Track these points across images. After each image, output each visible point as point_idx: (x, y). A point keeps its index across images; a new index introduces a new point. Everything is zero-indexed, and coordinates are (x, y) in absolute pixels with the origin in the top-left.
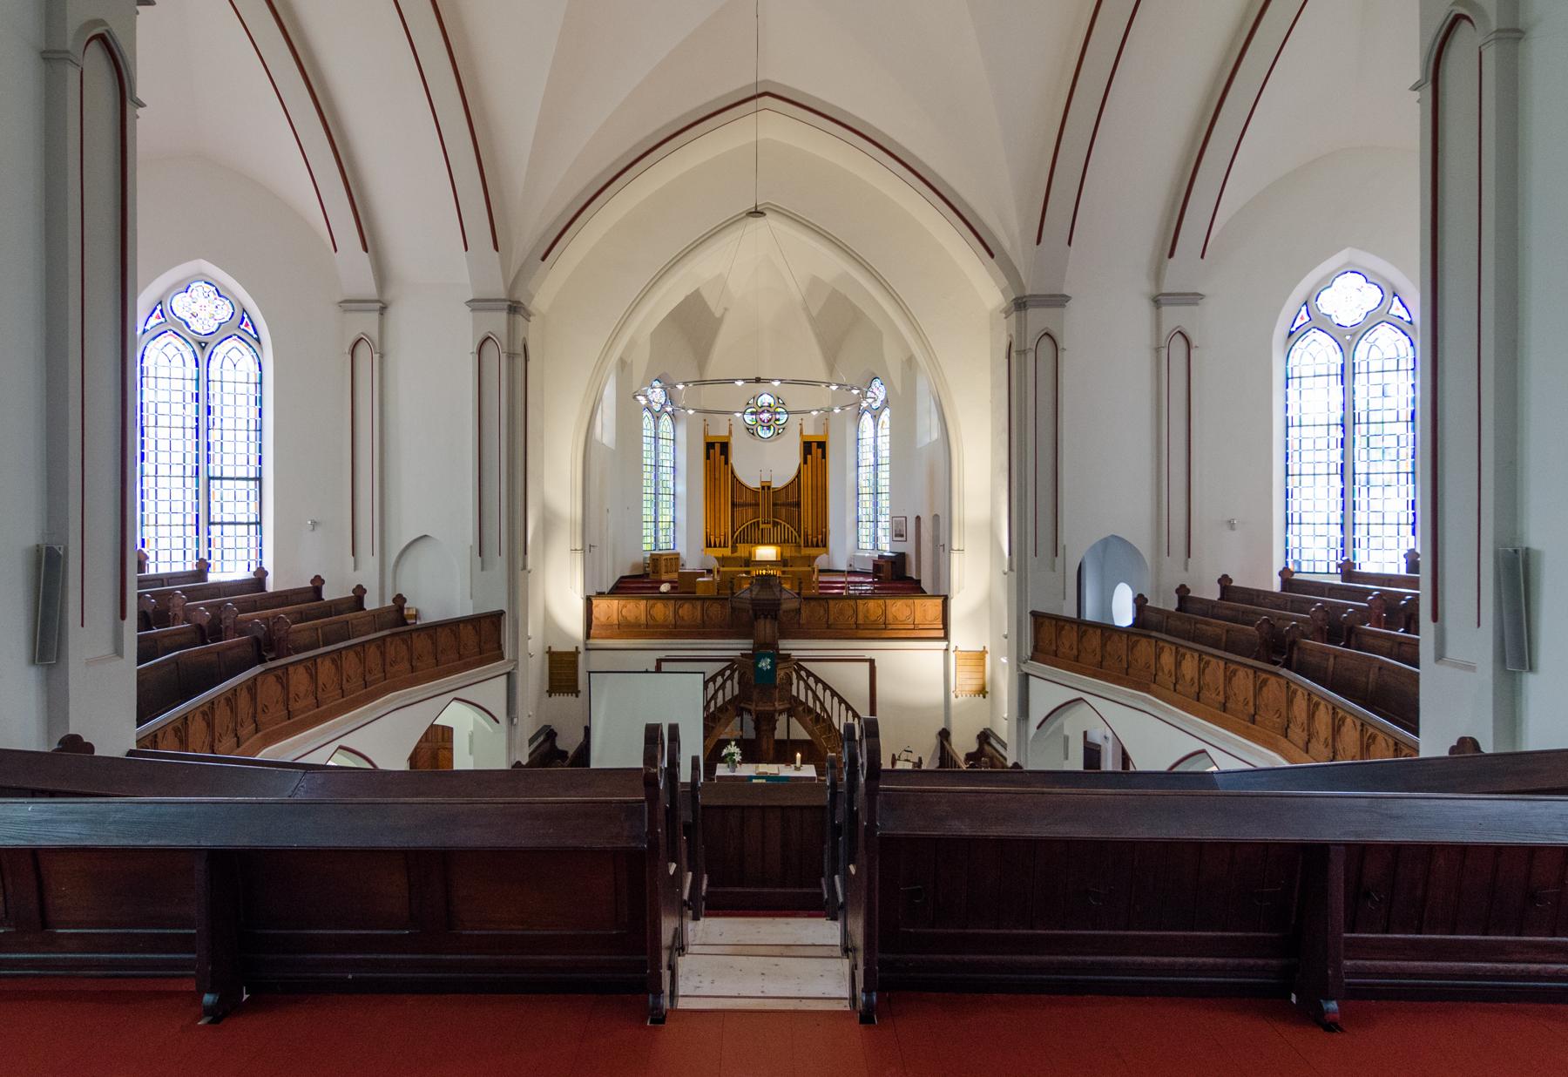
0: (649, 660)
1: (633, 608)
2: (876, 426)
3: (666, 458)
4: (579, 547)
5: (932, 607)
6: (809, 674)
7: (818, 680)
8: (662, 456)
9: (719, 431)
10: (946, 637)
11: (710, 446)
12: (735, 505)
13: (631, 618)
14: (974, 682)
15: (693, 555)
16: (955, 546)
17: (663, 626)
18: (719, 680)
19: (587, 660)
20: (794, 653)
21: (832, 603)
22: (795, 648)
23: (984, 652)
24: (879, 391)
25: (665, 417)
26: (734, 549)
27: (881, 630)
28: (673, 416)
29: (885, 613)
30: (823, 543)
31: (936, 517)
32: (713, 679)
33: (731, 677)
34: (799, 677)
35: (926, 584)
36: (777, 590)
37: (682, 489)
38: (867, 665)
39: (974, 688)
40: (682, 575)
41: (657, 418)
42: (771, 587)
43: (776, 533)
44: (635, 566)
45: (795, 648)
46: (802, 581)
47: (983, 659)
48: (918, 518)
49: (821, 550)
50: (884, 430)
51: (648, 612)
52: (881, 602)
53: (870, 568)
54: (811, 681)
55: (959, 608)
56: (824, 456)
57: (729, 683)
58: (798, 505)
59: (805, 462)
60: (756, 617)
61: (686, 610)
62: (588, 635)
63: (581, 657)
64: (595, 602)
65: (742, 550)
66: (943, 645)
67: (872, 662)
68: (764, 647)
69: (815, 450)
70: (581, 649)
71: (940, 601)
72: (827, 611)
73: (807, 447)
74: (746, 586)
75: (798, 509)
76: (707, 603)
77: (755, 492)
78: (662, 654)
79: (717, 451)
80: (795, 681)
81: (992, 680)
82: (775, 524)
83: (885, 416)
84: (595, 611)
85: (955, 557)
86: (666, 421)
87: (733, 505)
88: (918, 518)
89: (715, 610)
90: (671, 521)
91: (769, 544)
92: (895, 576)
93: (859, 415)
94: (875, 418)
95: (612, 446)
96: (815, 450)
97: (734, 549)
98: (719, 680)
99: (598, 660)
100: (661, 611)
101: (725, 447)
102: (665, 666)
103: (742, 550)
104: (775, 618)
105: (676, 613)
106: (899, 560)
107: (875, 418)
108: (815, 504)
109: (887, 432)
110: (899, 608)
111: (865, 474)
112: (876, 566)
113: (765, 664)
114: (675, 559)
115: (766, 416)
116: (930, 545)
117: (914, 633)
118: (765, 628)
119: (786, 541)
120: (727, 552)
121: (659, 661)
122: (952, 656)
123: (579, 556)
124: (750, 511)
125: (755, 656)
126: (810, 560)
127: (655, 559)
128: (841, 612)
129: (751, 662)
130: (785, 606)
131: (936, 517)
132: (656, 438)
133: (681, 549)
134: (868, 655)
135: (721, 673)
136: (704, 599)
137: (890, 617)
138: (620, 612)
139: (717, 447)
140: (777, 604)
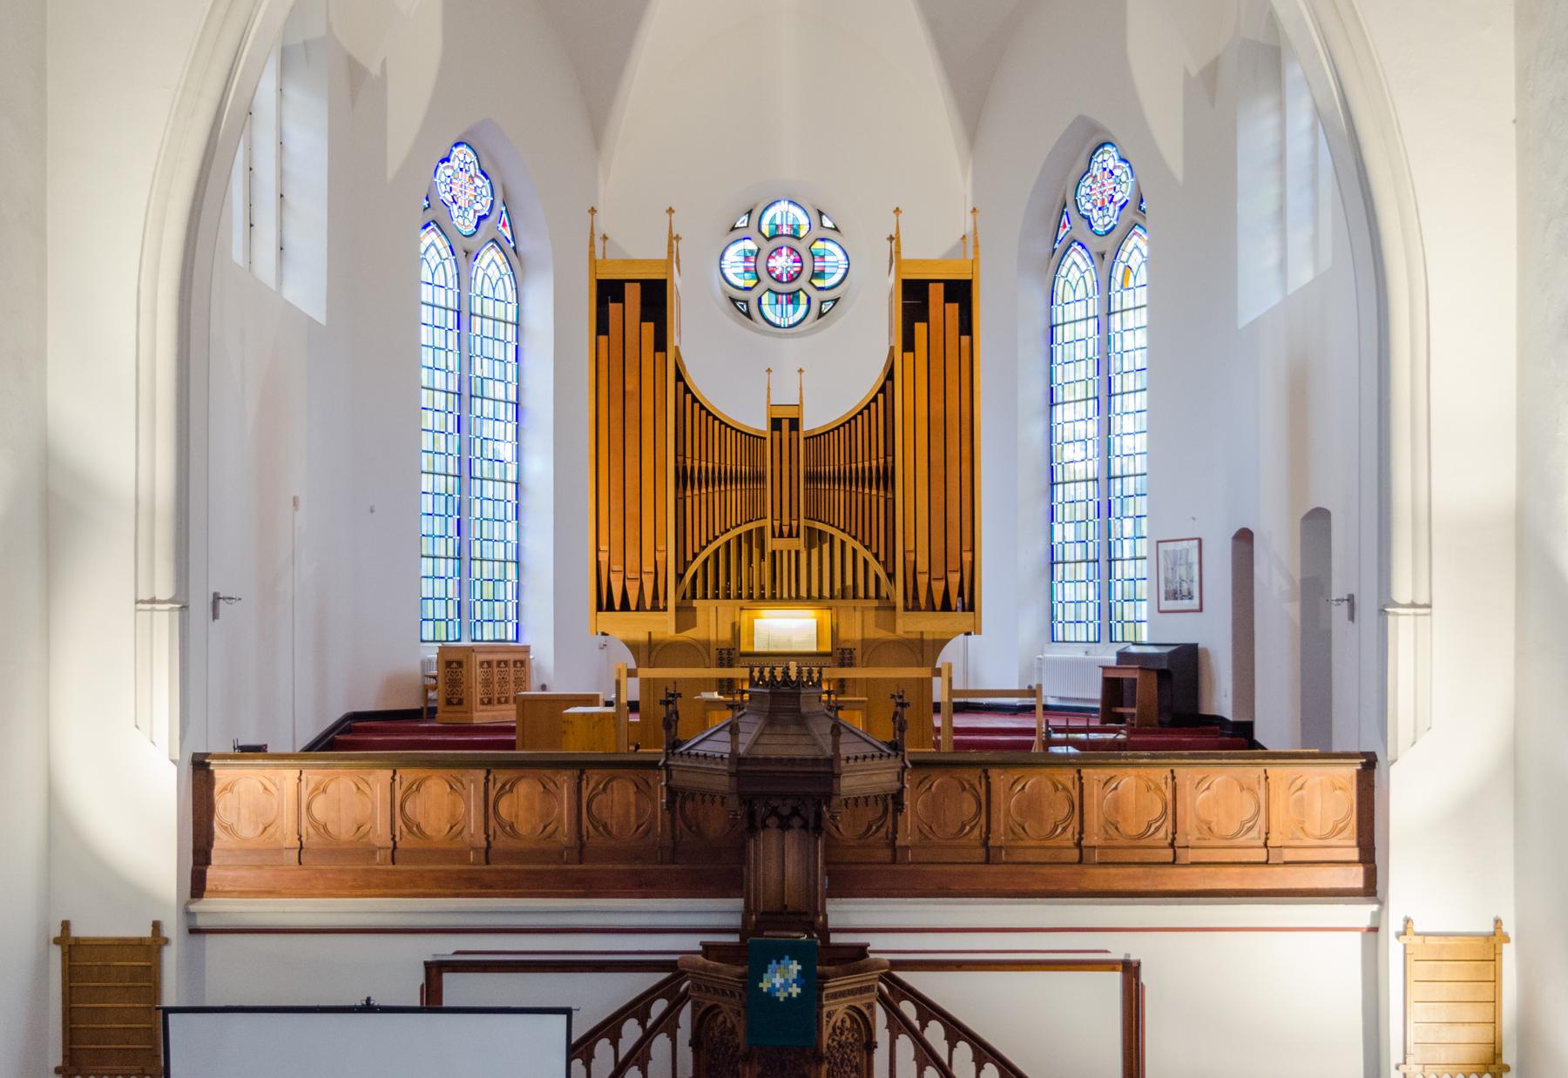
0: (397, 969)
1: (356, 796)
2: (1105, 285)
3: (492, 366)
4: (164, 589)
5: (1325, 792)
6: (929, 1010)
7: (956, 1031)
8: (481, 368)
9: (636, 249)
10: (1371, 889)
11: (609, 291)
12: (701, 488)
13: (343, 830)
14: (1464, 1034)
15: (568, 651)
16: (1402, 590)
17: (446, 855)
18: (631, 1032)
19: (194, 967)
20: (876, 942)
21: (1000, 779)
22: (878, 923)
23: (1495, 938)
24: (1109, 182)
25: (490, 255)
26: (685, 614)
27: (1155, 868)
28: (514, 255)
29: (1172, 811)
30: (962, 598)
31: (1317, 522)
32: (610, 1028)
33: (668, 1023)
34: (898, 1024)
35: (1275, 723)
36: (822, 729)
37: (540, 466)
38: (1115, 978)
39: (1464, 1054)
40: (528, 705)
41: (465, 255)
42: (801, 720)
43: (817, 567)
44: (394, 683)
45: (878, 923)
46: (907, 707)
47: (1494, 959)
48: (1244, 538)
49: (958, 619)
50: (1133, 297)
51: (396, 808)
52: (1159, 774)
53: (1093, 693)
54: (935, 1034)
55: (1408, 798)
56: (966, 327)
57: (661, 1044)
58: (886, 478)
59: (908, 344)
60: (753, 826)
61: (524, 805)
62: (198, 886)
63: (171, 959)
64: (223, 774)
65: (712, 621)
66: (1361, 913)
67: (1130, 970)
68: (785, 925)
69: (935, 306)
70: (172, 929)
71: (1348, 772)
72: (986, 805)
73: (914, 295)
74: (721, 718)
75: (880, 494)
76: (594, 776)
77: (751, 439)
78: (445, 947)
79: (633, 307)
80: (882, 1035)
81: (1527, 1030)
82: (815, 538)
83: (1136, 250)
84: (225, 807)
85: (1402, 627)
86: (491, 263)
87: (683, 478)
88: (1244, 538)
89: (619, 801)
90: (524, 570)
91: (797, 599)
92: (1163, 705)
93: (1057, 256)
94: (1104, 260)
95: (320, 317)
96: (935, 306)
97: (685, 614)
98: (631, 1032)
99: (232, 970)
100: (443, 802)
101: (655, 297)
102: (456, 988)
103: (712, 621)
104: (815, 827)
105: (489, 808)
106: (1178, 671)
107: (1104, 260)
108: (938, 474)
109: (1142, 296)
110: (1213, 791)
111: (1075, 419)
112: (1114, 688)
113: (782, 979)
114: (516, 662)
115: (782, 263)
116: (1293, 610)
117: (1258, 878)
118: (781, 859)
119: (847, 594)
120: (662, 626)
121: (435, 970)
122: (1394, 951)
123: (164, 622)
124: (735, 495)
125: (749, 951)
126: (925, 650)
127: (453, 664)
128: (1031, 807)
129: (731, 972)
130: (851, 783)
131: (1317, 522)
132: (462, 316)
133: (541, 645)
134: (1119, 947)
135: (637, 1008)
136: (581, 766)
137: (1189, 832)
138: (303, 808)
139: (633, 294)
140: (825, 773)
